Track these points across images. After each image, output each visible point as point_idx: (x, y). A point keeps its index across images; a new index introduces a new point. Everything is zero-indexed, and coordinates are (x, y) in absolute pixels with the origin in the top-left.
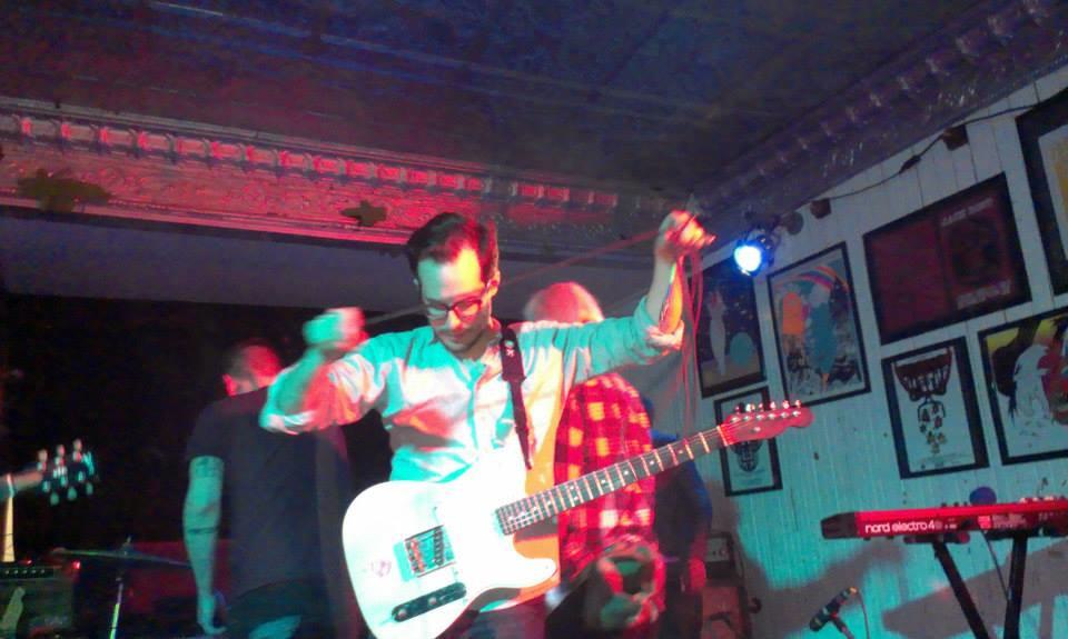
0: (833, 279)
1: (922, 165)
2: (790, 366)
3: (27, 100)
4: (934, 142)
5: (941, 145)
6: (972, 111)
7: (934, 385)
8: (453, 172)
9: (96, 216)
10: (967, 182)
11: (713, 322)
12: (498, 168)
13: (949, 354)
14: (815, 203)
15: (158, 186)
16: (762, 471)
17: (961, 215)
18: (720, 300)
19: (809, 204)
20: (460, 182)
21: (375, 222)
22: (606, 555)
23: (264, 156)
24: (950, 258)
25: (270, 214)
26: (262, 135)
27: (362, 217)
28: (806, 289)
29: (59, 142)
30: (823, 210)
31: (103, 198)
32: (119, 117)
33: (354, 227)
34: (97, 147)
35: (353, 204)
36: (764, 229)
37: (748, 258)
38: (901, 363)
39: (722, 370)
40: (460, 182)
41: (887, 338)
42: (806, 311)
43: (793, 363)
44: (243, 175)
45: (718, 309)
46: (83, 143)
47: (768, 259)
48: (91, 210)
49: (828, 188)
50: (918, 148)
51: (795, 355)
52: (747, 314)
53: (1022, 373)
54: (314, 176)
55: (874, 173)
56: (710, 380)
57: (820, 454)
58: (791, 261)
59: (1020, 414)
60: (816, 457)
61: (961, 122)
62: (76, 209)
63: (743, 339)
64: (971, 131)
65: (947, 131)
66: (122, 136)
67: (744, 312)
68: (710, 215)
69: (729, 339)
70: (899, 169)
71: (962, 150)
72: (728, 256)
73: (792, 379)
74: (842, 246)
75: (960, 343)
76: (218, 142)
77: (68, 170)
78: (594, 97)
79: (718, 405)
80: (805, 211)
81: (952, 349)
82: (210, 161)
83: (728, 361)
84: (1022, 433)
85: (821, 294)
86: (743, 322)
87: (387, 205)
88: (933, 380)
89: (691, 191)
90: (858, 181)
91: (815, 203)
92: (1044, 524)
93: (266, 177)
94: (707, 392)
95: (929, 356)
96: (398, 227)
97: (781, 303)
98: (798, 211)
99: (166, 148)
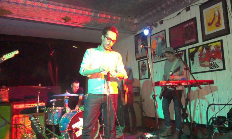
0: (162, 37)
4: (184, 9)
5: (185, 11)
12: (95, 10)
13: (183, 53)
14: (160, 21)
16: (146, 75)
17: (187, 25)
18: (140, 41)
20: (87, 13)
21: (69, 21)
27: (65, 20)
28: (157, 39)
30: (162, 23)
31: (10, 13)
33: (64, 22)
35: (64, 17)
36: (151, 26)
37: (146, 32)
39: (140, 55)
42: (157, 43)
47: (150, 32)
48: (8, 16)
50: (181, 11)
54: (55, 10)
56: (138, 57)
58: (155, 33)
59: (194, 65)
60: (157, 72)
61: (189, 6)
62: (5, 15)
64: (191, 7)
67: (145, 43)
68: (139, 23)
70: (177, 15)
71: (189, 12)
73: (153, 57)
74: (165, 30)
75: (185, 51)
79: (139, 62)
80: (158, 23)
81: (183, 52)
85: (160, 40)
90: (169, 17)
94: (137, 59)
95: (142, 59)
98: (157, 23)
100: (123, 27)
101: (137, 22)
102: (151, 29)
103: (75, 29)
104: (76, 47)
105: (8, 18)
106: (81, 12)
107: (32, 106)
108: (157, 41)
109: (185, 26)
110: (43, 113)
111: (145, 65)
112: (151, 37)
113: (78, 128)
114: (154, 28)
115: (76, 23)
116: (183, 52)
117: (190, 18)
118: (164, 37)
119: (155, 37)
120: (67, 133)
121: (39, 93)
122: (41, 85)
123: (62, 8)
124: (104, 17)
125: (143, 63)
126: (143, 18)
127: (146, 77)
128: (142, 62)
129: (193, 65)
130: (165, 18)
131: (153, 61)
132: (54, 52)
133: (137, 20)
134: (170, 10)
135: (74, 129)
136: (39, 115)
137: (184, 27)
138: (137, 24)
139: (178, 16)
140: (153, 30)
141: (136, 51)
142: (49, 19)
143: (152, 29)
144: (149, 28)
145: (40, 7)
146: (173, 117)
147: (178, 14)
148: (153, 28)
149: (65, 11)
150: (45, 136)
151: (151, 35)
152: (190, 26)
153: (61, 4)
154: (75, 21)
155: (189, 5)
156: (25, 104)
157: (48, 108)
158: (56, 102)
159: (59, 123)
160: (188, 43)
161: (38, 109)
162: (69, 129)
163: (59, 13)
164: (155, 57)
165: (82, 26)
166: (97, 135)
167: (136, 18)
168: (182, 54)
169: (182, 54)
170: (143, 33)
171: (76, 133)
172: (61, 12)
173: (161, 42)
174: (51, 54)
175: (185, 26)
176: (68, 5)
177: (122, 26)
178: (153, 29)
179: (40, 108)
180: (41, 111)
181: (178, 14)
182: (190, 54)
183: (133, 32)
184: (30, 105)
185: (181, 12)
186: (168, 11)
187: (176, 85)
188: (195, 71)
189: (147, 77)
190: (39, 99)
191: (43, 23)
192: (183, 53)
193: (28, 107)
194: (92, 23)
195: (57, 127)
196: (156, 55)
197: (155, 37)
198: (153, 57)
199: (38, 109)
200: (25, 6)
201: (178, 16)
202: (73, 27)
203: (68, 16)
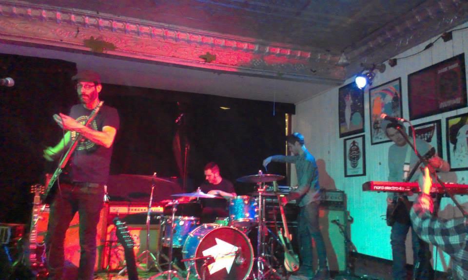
0: (394, 93)
1: (433, 48)
2: (374, 127)
3: (87, 11)
4: (438, 39)
5: (441, 40)
6: (455, 26)
7: (427, 138)
8: (243, 42)
9: (113, 55)
10: (449, 56)
11: (347, 107)
12: (261, 40)
13: (434, 126)
14: (390, 60)
15: (133, 44)
16: (359, 168)
17: (445, 70)
18: (350, 98)
19: (388, 61)
20: (245, 46)
21: (212, 61)
22: (444, 226)
23: (171, 34)
24: (437, 88)
25: (173, 56)
26: (171, 25)
27: (207, 59)
28: (384, 96)
29: (97, 26)
30: (394, 63)
31: (113, 48)
32: (120, 18)
33: (204, 63)
34: (111, 29)
35: (203, 53)
36: (369, 72)
37: (361, 82)
38: (416, 129)
39: (348, 128)
40: (245, 46)
41: (412, 118)
42: (383, 105)
43: (375, 126)
44: (163, 41)
45: (349, 101)
46: (106, 27)
47: (369, 82)
48: (109, 52)
49: (397, 54)
50: (433, 40)
51: (377, 123)
52: (360, 105)
53: (460, 135)
54: (189, 42)
55: (415, 50)
56: (343, 131)
57: (382, 163)
58: (379, 84)
59: (457, 154)
60: (380, 164)
61: (449, 31)
62: (104, 52)
63: (357, 115)
64: (454, 34)
65: (444, 34)
66: (120, 25)
67: (359, 104)
68: (349, 63)
69: (352, 114)
70: (424, 48)
71: (449, 43)
72: (353, 81)
73: (374, 132)
74: (400, 79)
75: (439, 122)
76: (155, 28)
77: (101, 37)
78: (298, 14)
79: (345, 140)
80: (386, 63)
81: (436, 124)
82: (151, 35)
83: (351, 123)
84: (457, 159)
85: (389, 99)
86: (358, 108)
87: (217, 54)
88: (427, 136)
89: (343, 52)
90: (409, 52)
91: (390, 60)
92: (446, 193)
93: (171, 42)
94: (342, 136)
95: (427, 126)
96: (220, 63)
97: (374, 100)
98: (384, 63)
99: (136, 30)
100: (315, 71)
101: (345, 61)
102: (371, 75)
103: (223, 75)
104: (226, 107)
105: (108, 56)
106: (234, 44)
107: (140, 211)
108: (384, 99)
109: (440, 72)
110: (156, 226)
111: (358, 149)
112: (373, 92)
113: (213, 258)
114: (378, 74)
115: (224, 65)
116: (436, 124)
117: (452, 56)
118: (398, 92)
119: (380, 93)
120: (193, 264)
121: (153, 188)
122: (156, 175)
123: (200, 37)
124: (278, 52)
125: (354, 143)
126: (356, 52)
127: (357, 172)
128: (351, 141)
129: (455, 154)
130: (401, 55)
131: (375, 141)
132: (182, 117)
133: (345, 57)
134: (411, 38)
135: (206, 258)
136: (150, 229)
137: (439, 73)
138: (344, 65)
139: (426, 50)
140: (375, 77)
141: (341, 118)
142: (178, 57)
143: (373, 75)
144: (368, 75)
145: (163, 37)
146: (410, 260)
147: (428, 47)
148: (375, 74)
149: (205, 44)
150: (158, 268)
151: (371, 87)
152: (449, 72)
153: (200, 31)
154: (224, 60)
155: (450, 28)
156: (129, 206)
157: (167, 217)
158: (178, 206)
159: (182, 246)
160: (446, 106)
161: (149, 218)
162: (196, 257)
163: (196, 47)
164: (377, 133)
165: (235, 70)
166: (248, 276)
167: (343, 54)
168: (433, 128)
169: (433, 128)
170: (354, 83)
171: (210, 267)
172: (198, 46)
173: (391, 102)
174: (177, 121)
175: (440, 72)
176: (212, 33)
177: (314, 70)
178: (377, 75)
179: (153, 215)
180: (154, 221)
181: (428, 47)
182: (449, 130)
183: (337, 82)
184: (137, 208)
185: (434, 42)
186: (408, 40)
187: (408, 191)
188: (459, 165)
189: (361, 172)
190: (151, 198)
191: (168, 64)
192: (434, 126)
193: (134, 212)
194: (255, 64)
195: (177, 252)
196: (380, 128)
197: (380, 93)
198: (374, 132)
199: (149, 218)
200: (139, 35)
201: (428, 50)
202: (220, 72)
203: (210, 52)
